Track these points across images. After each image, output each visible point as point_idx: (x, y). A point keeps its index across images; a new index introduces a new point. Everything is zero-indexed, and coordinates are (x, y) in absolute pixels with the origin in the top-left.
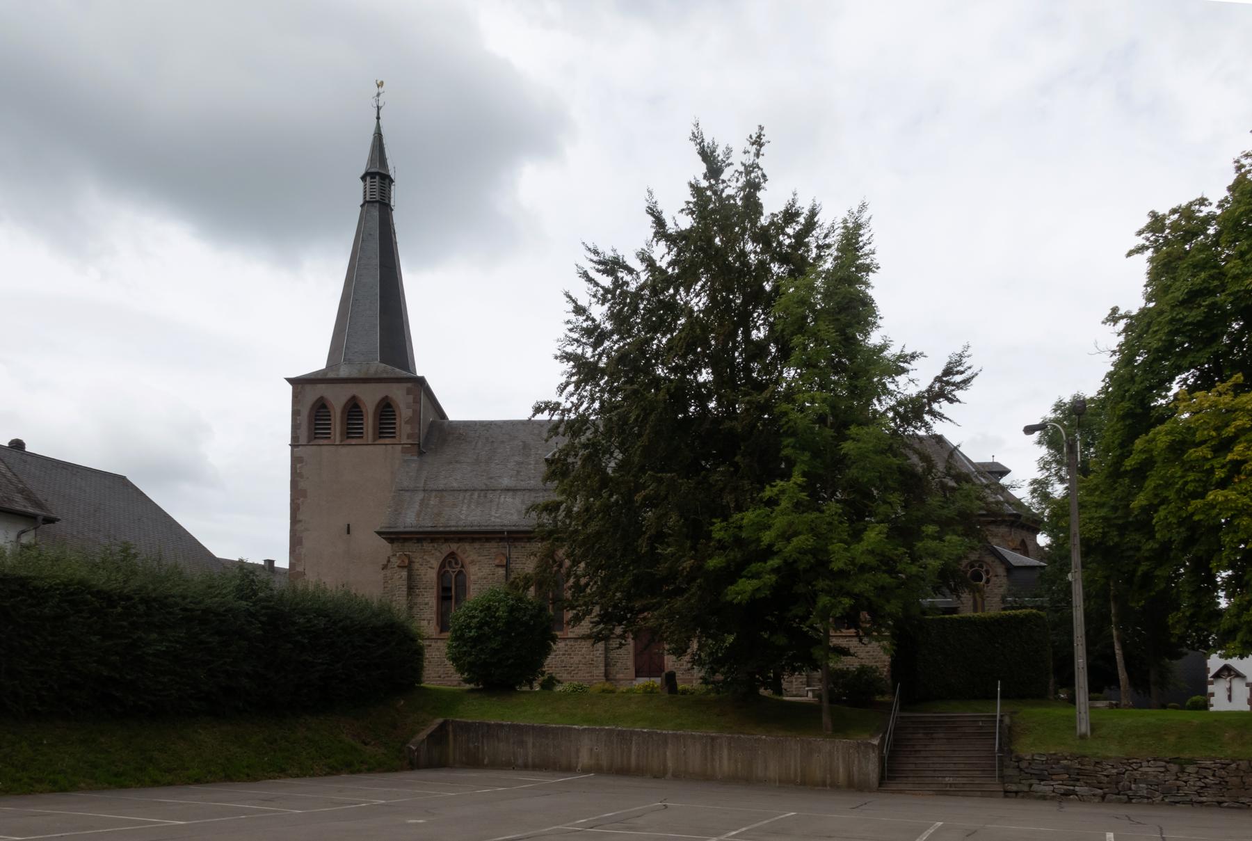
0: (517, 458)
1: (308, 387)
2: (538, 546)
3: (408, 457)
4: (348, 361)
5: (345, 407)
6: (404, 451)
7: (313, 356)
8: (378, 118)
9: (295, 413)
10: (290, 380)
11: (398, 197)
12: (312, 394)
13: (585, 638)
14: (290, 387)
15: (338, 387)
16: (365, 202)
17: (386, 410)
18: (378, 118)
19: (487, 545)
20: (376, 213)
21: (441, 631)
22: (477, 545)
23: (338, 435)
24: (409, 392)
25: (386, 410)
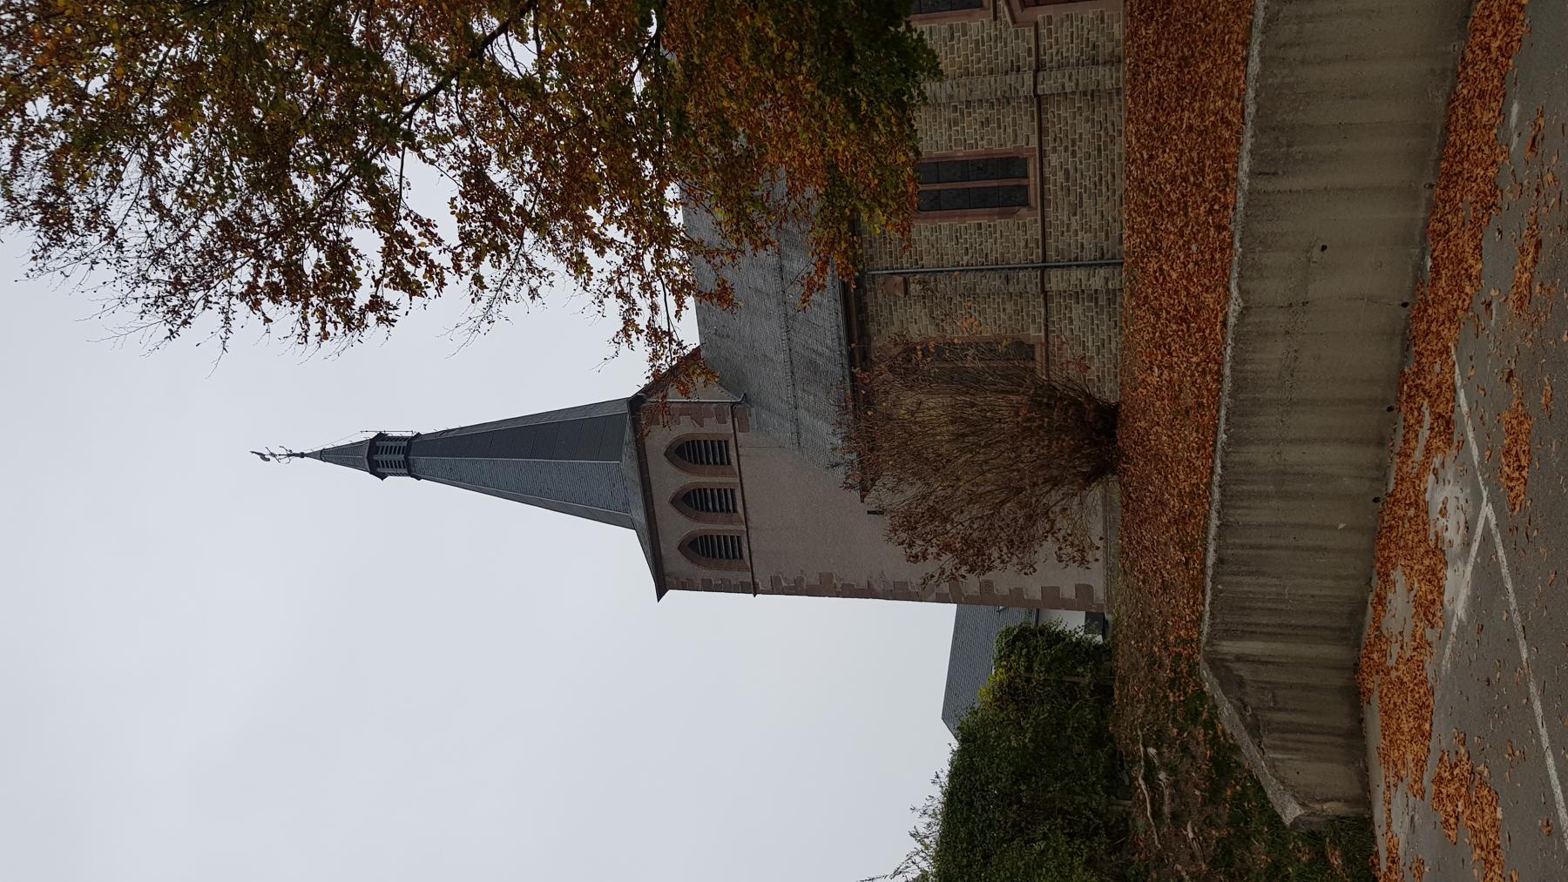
0: (68, 106)
2: (876, 224)
3: (752, 421)
5: (689, 516)
6: (745, 427)
7: (618, 550)
9: (708, 587)
10: (660, 595)
12: (677, 563)
14: (670, 593)
17: (687, 453)
19: (871, 309)
24: (653, 421)
25: (687, 453)
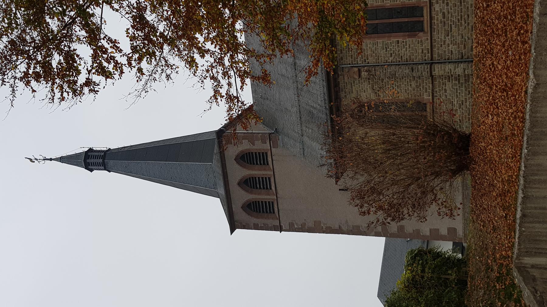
1: (236, 218)
3: (280, 143)
4: (215, 185)
5: (247, 191)
6: (276, 146)
8: (51, 159)
9: (256, 227)
10: (232, 231)
11: (100, 145)
12: (241, 215)
13: (158, 160)
14: (237, 231)
15: (233, 196)
16: (105, 169)
17: (246, 159)
18: (51, 159)
19: (341, 85)
20: (111, 163)
21: (422, 30)
22: (342, 95)
23: (268, 197)
24: (229, 142)
25: (246, 159)
